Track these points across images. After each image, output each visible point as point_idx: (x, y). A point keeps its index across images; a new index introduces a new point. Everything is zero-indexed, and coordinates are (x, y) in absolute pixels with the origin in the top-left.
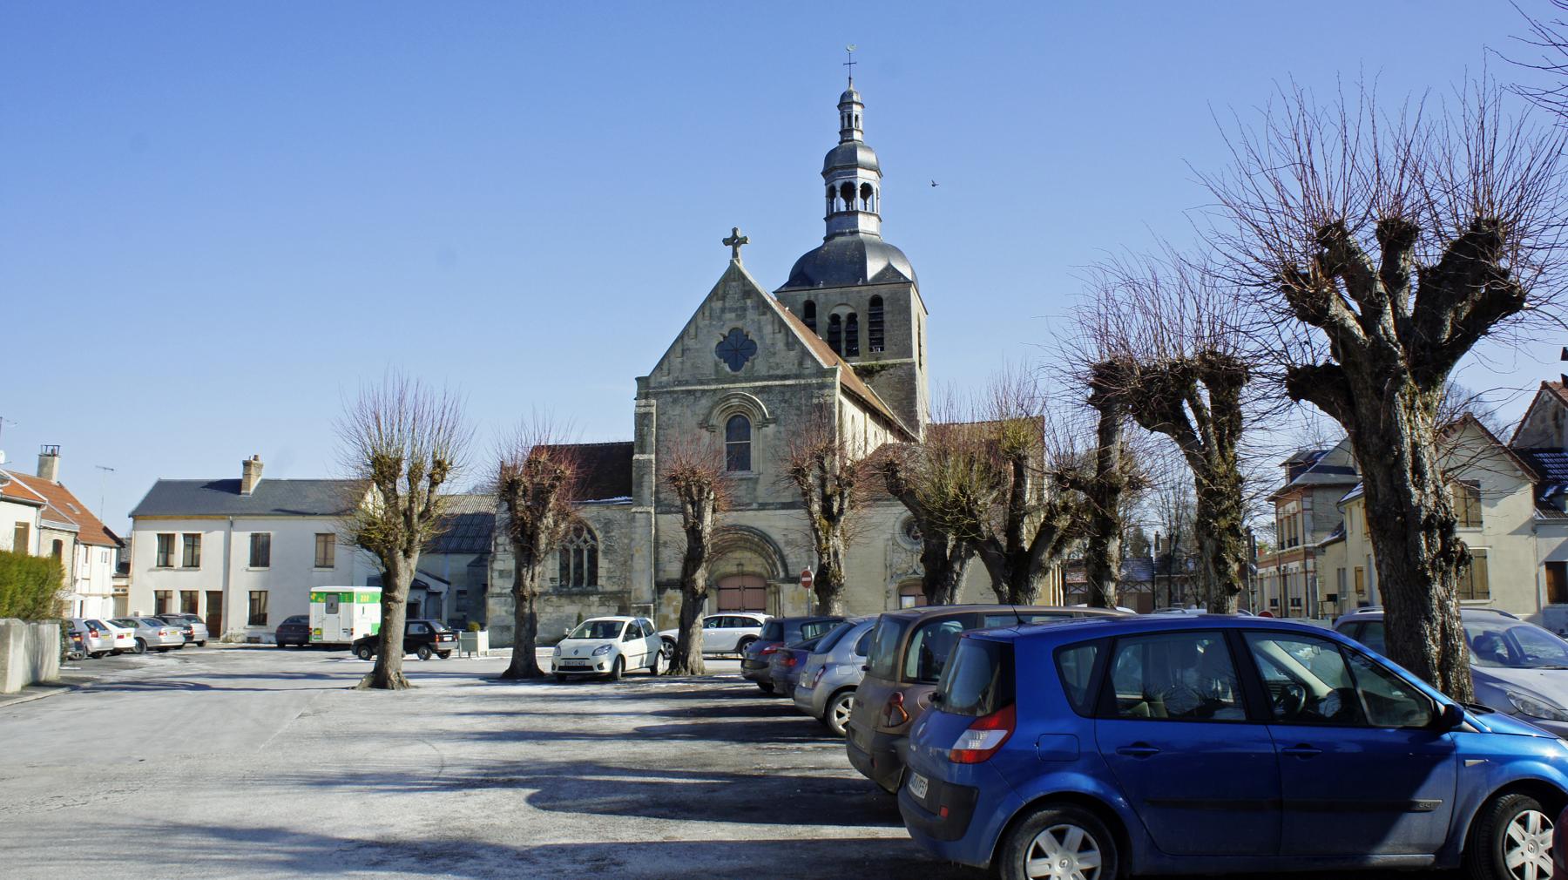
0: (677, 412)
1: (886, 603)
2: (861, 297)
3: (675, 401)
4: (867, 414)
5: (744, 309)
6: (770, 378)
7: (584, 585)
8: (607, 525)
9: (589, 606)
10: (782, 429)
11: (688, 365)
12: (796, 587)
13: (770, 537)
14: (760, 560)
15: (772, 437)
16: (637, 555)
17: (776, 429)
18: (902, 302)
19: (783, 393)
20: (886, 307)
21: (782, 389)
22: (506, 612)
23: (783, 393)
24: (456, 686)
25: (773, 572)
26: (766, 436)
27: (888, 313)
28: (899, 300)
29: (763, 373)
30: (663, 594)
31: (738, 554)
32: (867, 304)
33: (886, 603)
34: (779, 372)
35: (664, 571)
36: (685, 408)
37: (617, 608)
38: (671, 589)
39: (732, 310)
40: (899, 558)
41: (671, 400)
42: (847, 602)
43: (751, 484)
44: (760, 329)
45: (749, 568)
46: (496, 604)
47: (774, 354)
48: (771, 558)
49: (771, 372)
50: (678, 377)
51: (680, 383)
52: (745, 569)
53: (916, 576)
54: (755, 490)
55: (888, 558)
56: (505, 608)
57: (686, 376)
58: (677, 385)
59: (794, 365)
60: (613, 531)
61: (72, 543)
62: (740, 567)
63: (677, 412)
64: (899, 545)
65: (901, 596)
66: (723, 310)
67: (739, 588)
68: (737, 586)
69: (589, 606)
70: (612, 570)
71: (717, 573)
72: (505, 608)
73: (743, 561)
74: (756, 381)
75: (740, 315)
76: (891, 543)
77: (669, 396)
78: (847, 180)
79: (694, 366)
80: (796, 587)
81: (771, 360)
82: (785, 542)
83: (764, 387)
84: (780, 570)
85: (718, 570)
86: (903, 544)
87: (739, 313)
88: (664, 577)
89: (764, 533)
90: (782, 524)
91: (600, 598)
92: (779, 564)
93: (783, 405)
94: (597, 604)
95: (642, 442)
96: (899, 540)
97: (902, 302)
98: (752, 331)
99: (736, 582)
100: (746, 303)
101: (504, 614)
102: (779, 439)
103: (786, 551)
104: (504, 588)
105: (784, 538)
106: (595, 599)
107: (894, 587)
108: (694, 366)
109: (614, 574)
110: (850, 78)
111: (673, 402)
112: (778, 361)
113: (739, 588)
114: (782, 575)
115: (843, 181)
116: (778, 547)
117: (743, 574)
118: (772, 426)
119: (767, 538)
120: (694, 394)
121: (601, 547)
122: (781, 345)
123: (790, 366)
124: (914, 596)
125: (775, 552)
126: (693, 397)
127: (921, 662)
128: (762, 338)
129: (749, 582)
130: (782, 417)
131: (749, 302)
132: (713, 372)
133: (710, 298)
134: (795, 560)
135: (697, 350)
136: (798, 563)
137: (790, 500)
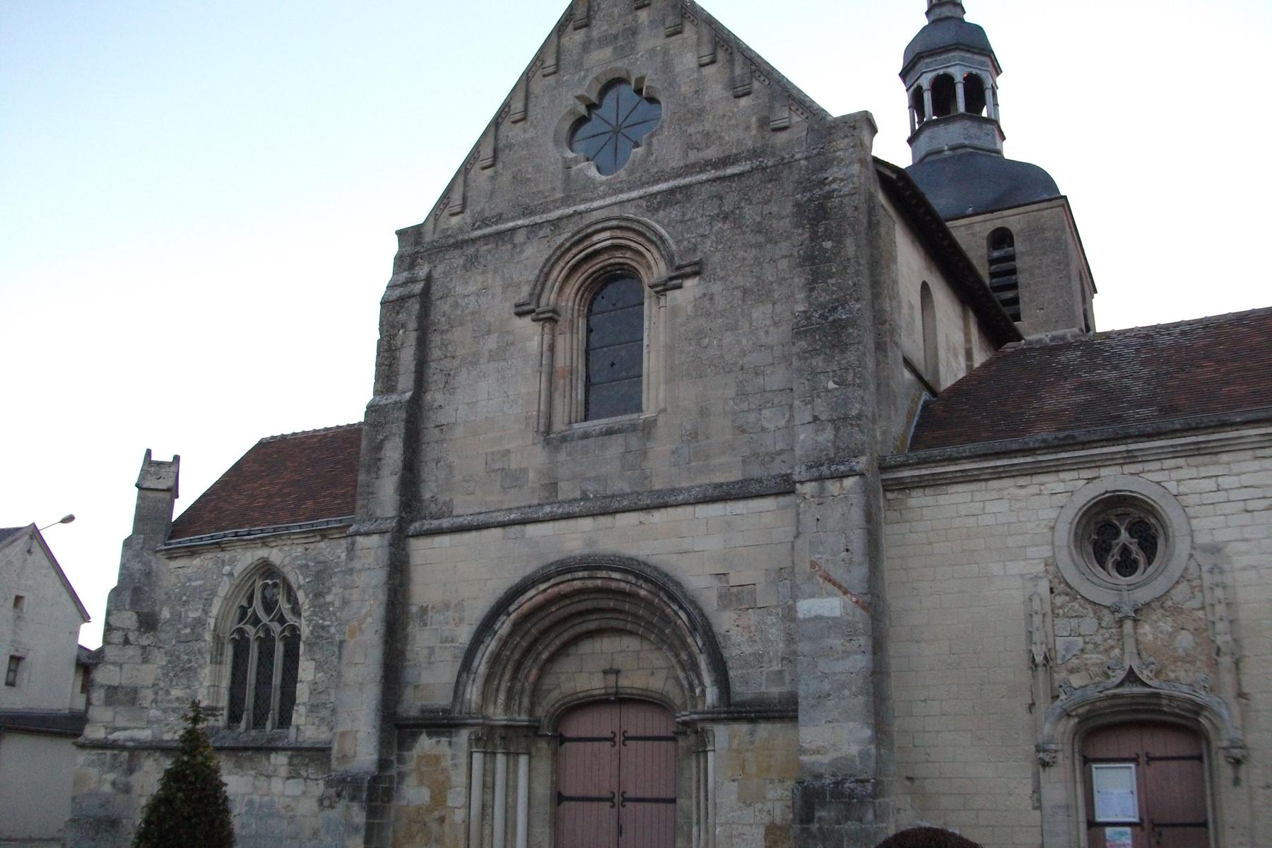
0: (472, 288)
2: (973, 235)
3: (472, 262)
4: (971, 314)
5: (633, 32)
7: (269, 725)
8: (321, 575)
9: (268, 777)
10: (716, 287)
13: (678, 584)
14: (658, 659)
16: (351, 643)
17: (700, 291)
18: (1048, 234)
19: (721, 198)
20: (1019, 246)
22: (114, 784)
24: (707, 819)
25: (692, 688)
26: (674, 312)
28: (1043, 230)
29: (673, 164)
30: (410, 748)
31: (607, 645)
33: (1037, 790)
34: (712, 153)
35: (416, 687)
36: (490, 275)
37: (321, 783)
38: (430, 735)
39: (605, 41)
41: (461, 262)
42: (911, 779)
44: (667, 66)
45: (634, 681)
47: (700, 113)
48: (685, 646)
49: (693, 156)
50: (482, 211)
52: (624, 682)
54: (644, 454)
55: (1037, 637)
56: (111, 776)
57: (500, 205)
58: (479, 228)
59: (748, 128)
60: (329, 589)
61: (108, 683)
62: (612, 678)
63: (472, 288)
64: (1072, 593)
65: (1087, 761)
66: (586, 47)
69: (268, 777)
70: (321, 688)
72: (111, 776)
74: (656, 182)
75: (622, 48)
76: (1044, 586)
77: (457, 252)
78: (941, 72)
80: (752, 734)
81: (691, 130)
83: (672, 191)
84: (707, 678)
86: (1086, 589)
88: (412, 704)
91: (291, 758)
92: (702, 661)
93: (718, 225)
94: (284, 771)
96: (1072, 576)
97: (1048, 234)
103: (724, 622)
104: (116, 729)
105: (716, 583)
107: (1060, 732)
109: (323, 698)
111: (464, 266)
112: (708, 127)
113: (611, 739)
115: (935, 73)
116: (697, 607)
118: (689, 283)
119: (673, 589)
120: (511, 239)
121: (305, 631)
122: (716, 90)
124: (1135, 760)
125: (693, 629)
126: (509, 247)
128: (672, 83)
129: (637, 721)
130: (717, 257)
131: (643, 15)
132: (559, 184)
133: (560, 28)
134: (748, 649)
135: (527, 144)
136: (758, 657)
137: (734, 475)
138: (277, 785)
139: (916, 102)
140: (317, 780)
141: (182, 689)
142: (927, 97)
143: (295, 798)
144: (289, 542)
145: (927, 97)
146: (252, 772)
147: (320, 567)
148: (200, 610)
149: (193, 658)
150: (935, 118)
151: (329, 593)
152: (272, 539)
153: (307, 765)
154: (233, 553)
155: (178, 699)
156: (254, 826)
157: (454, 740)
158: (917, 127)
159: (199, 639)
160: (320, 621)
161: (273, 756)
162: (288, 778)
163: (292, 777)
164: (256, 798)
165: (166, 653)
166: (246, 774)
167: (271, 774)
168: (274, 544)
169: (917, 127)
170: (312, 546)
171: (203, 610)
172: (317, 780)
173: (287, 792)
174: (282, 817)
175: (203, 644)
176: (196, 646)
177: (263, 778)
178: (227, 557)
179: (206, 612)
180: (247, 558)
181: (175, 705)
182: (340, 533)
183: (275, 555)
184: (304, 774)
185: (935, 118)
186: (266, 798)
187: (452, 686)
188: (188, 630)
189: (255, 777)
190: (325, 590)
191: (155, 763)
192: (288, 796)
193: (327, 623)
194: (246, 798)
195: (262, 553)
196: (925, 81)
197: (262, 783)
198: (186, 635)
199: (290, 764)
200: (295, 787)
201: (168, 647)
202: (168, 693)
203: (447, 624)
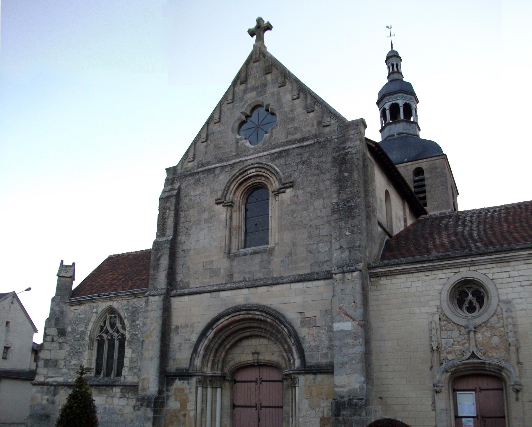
0: (197, 192)
1: (434, 403)
2: (407, 170)
3: (197, 182)
4: (406, 204)
5: (265, 85)
6: (288, 143)
7: (112, 376)
8: (134, 313)
10: (300, 192)
11: (212, 146)
12: (314, 379)
13: (284, 317)
14: (275, 348)
15: (288, 202)
16: (147, 341)
18: (438, 170)
19: (301, 155)
20: (426, 175)
21: (299, 151)
22: (48, 400)
23: (301, 155)
25: (289, 360)
26: (282, 203)
27: (428, 178)
28: (436, 168)
30: (171, 386)
31: (254, 342)
32: (412, 174)
33: (434, 403)
34: (298, 136)
35: (174, 360)
36: (205, 187)
37: (134, 400)
38: (180, 380)
39: (253, 89)
40: (449, 337)
41: (193, 181)
43: (265, 257)
44: (279, 100)
45: (265, 357)
46: (38, 392)
47: (293, 119)
48: (287, 342)
49: (290, 137)
50: (200, 161)
51: (203, 165)
52: (261, 358)
53: (476, 361)
54: (269, 262)
57: (209, 158)
58: (200, 167)
59: (313, 126)
62: (256, 356)
63: (197, 192)
64: (448, 320)
65: (454, 390)
66: (245, 92)
67: (256, 382)
68: (254, 379)
69: (112, 397)
70: (134, 360)
71: (232, 363)
72: (46, 397)
73: (259, 349)
74: (274, 148)
75: (260, 92)
76: (437, 318)
78: (394, 102)
79: (217, 147)
81: (289, 126)
82: (301, 322)
83: (281, 152)
85: (233, 359)
86: (454, 319)
87: (260, 90)
88: (172, 367)
89: (279, 313)
90: (298, 300)
91: (121, 389)
92: (294, 349)
93: (300, 166)
94: (119, 395)
95: (163, 225)
96: (448, 313)
97: (438, 170)
98: (272, 102)
99: (252, 374)
100: (266, 79)
101: (45, 402)
102: (296, 204)
103: (303, 332)
104: (49, 377)
106: (117, 390)
107: (443, 378)
108: (217, 147)
109: (135, 364)
110: (392, 44)
111: (194, 184)
112: (296, 125)
114: (298, 363)
115: (391, 103)
116: (292, 326)
117: (260, 365)
118: (288, 191)
119: (282, 318)
122: (299, 110)
123: (309, 128)
124: (475, 390)
125: (290, 335)
126: (213, 175)
127: (269, 55)
129: (267, 374)
130: (300, 180)
131: (269, 77)
132: (234, 149)
134: (313, 344)
136: (317, 347)
137: (307, 271)
138: (116, 401)
139: (383, 115)
140: (132, 398)
141: (76, 361)
142: (388, 113)
143: (124, 406)
144: (121, 299)
145: (388, 113)
146: (106, 395)
147: (134, 309)
148: (84, 328)
149: (81, 348)
150: (391, 121)
151: (137, 320)
152: (114, 298)
153: (128, 392)
154: (97, 304)
155: (74, 365)
156: (106, 418)
157: (190, 382)
158: (384, 125)
159: (83, 339)
160: (134, 332)
161: (114, 388)
162: (120, 398)
163: (122, 397)
164: (107, 406)
165: (69, 345)
166: (103, 396)
167: (113, 396)
168: (115, 300)
169: (384, 125)
170: (130, 300)
171: (85, 327)
172: (132, 398)
173: (120, 404)
174: (118, 414)
175: (85, 342)
176: (82, 342)
177: (110, 398)
178: (95, 305)
179: (86, 328)
180: (103, 305)
181: (73, 367)
182: (142, 295)
183: (115, 304)
184: (127, 396)
185: (391, 121)
186: (111, 406)
187: (189, 359)
188: (79, 336)
189: (107, 397)
190: (136, 319)
191: (65, 391)
192: (121, 405)
193: (137, 333)
194: (103, 406)
195: (110, 303)
196: (387, 106)
197: (110, 399)
198: (78, 338)
199: (121, 392)
200: (123, 402)
201: (70, 343)
202: (70, 362)
203: (187, 333)
